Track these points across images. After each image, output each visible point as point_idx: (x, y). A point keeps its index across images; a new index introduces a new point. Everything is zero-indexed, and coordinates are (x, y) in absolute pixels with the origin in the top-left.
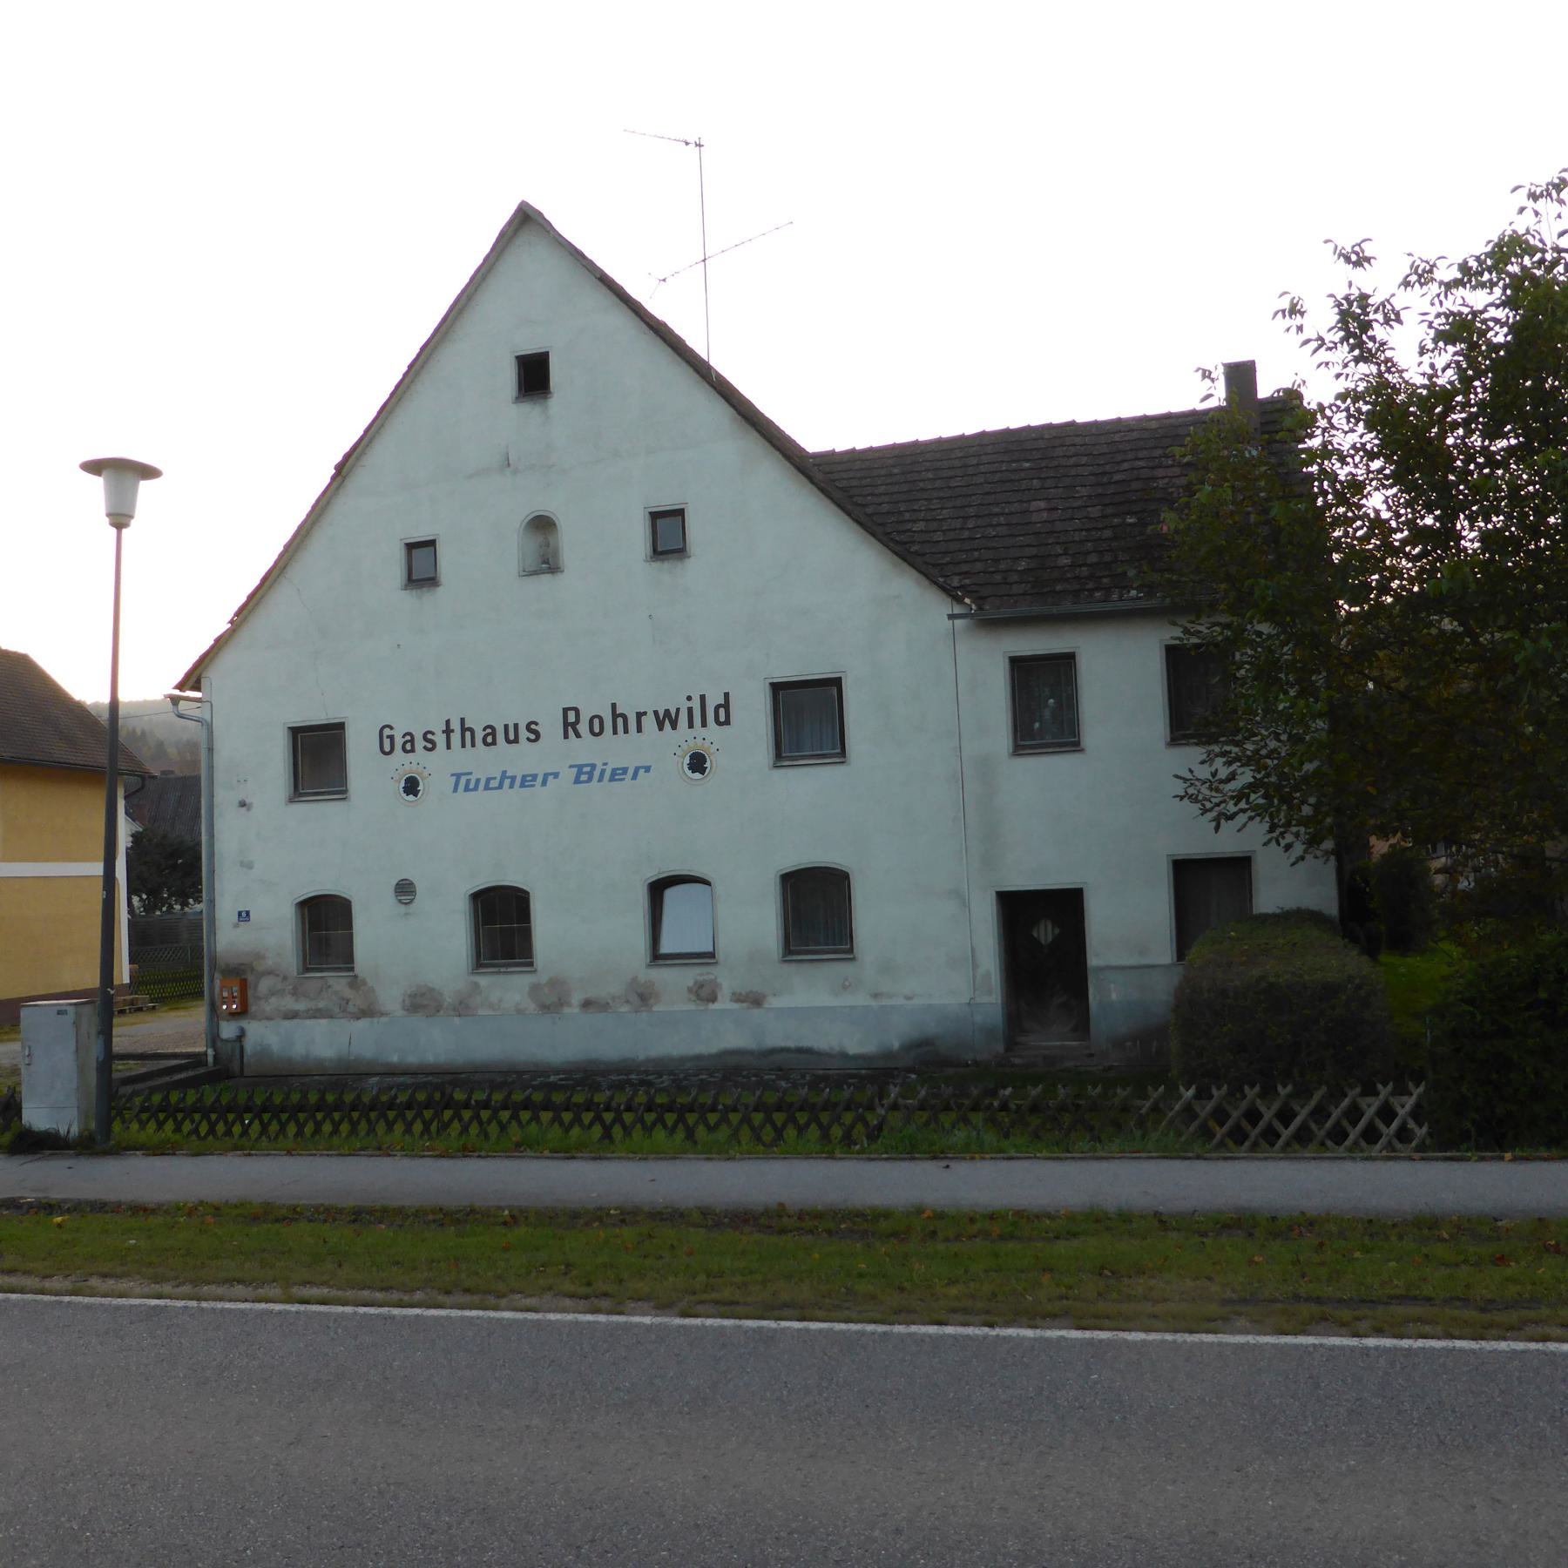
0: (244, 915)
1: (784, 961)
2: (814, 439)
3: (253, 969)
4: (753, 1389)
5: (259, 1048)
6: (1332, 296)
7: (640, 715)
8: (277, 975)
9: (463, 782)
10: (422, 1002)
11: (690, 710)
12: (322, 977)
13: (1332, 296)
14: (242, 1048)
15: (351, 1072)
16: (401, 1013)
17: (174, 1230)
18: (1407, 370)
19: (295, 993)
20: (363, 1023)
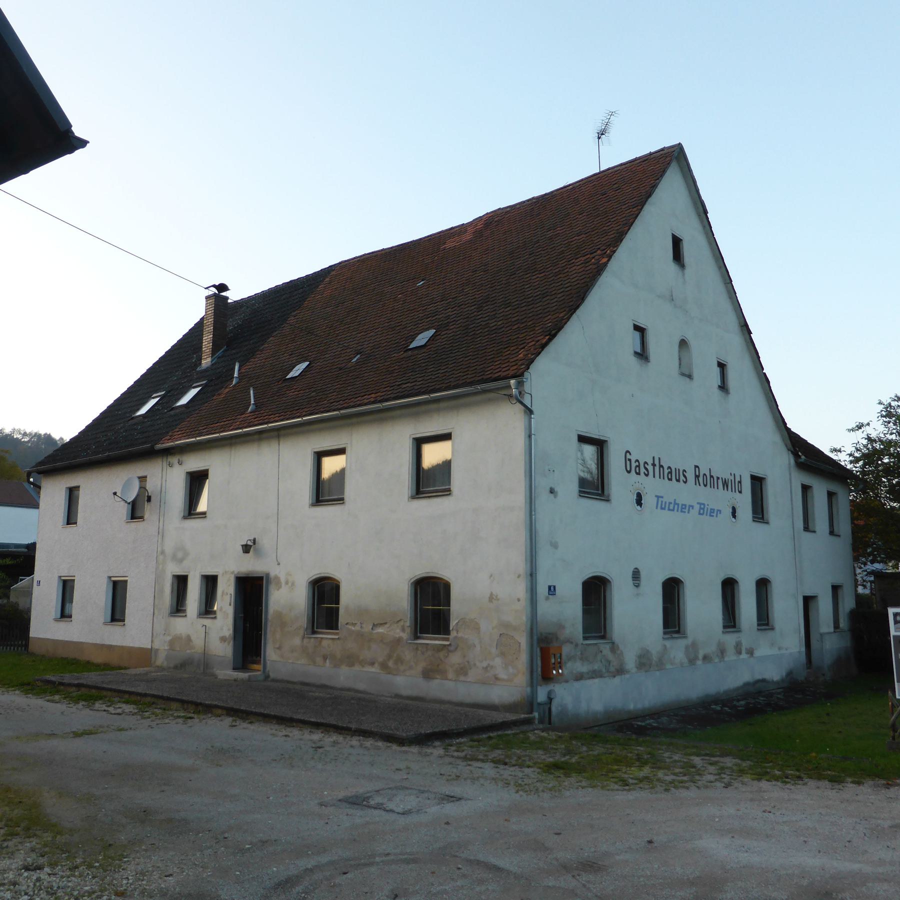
0: (552, 588)
1: (200, 617)
2: (794, 426)
3: (557, 638)
4: (770, 887)
5: (560, 708)
6: (863, 438)
7: (718, 478)
8: (572, 643)
9: (662, 505)
10: (645, 662)
11: (731, 480)
12: (596, 644)
13: (863, 438)
14: (550, 709)
15: (611, 721)
16: (634, 670)
17: (601, 831)
18: (868, 424)
19: (583, 659)
20: (617, 680)
